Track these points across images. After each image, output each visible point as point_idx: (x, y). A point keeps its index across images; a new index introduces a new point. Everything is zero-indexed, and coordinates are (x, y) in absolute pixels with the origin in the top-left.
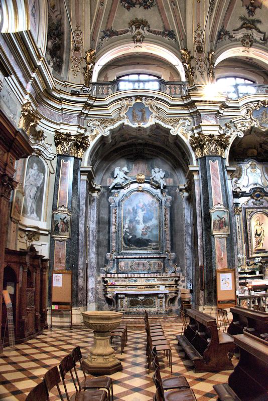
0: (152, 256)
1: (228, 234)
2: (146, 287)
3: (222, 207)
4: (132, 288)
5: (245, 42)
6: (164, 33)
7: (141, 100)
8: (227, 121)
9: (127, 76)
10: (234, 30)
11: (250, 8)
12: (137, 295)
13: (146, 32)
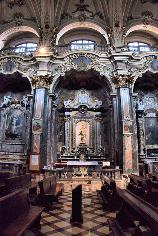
0: (18, 144)
1: (41, 133)
2: (12, 160)
3: (130, 118)
4: (5, 160)
5: (80, 19)
6: (31, 19)
7: (11, 59)
8: (56, 67)
10: (72, 13)
12: (5, 164)
13: (150, 19)
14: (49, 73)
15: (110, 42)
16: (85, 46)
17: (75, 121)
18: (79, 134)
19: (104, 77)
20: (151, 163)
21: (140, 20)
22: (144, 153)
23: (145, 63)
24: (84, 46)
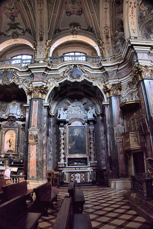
5: (14, 36)
9: (68, 54)
10: (7, 31)
11: (12, 18)
13: (79, 29)
14: (43, 84)
15: (102, 54)
16: (78, 58)
17: (4, 130)
18: (7, 142)
19: (96, 87)
20: (67, 172)
21: (69, 31)
22: (65, 161)
23: (64, 72)
24: (76, 58)
